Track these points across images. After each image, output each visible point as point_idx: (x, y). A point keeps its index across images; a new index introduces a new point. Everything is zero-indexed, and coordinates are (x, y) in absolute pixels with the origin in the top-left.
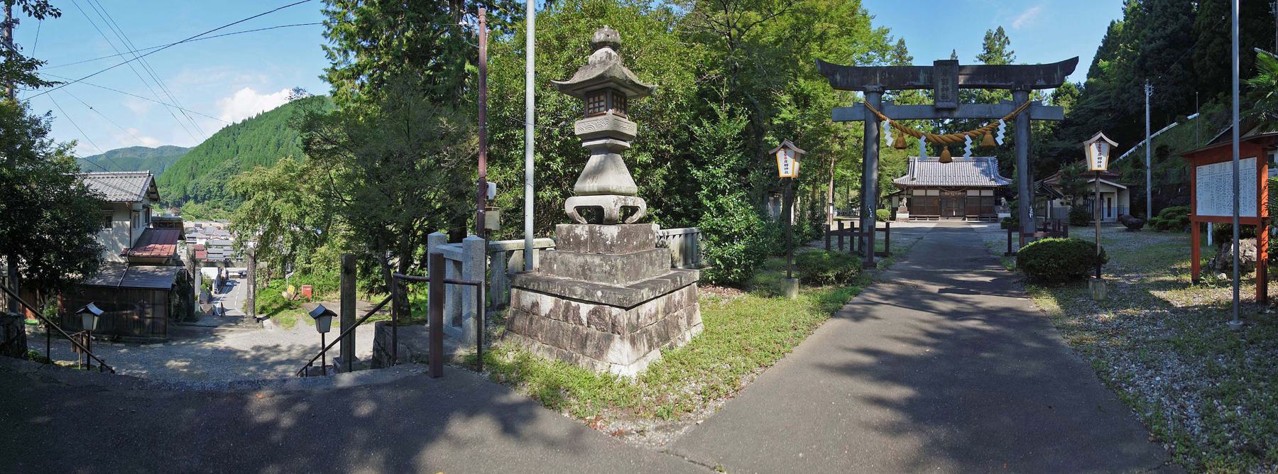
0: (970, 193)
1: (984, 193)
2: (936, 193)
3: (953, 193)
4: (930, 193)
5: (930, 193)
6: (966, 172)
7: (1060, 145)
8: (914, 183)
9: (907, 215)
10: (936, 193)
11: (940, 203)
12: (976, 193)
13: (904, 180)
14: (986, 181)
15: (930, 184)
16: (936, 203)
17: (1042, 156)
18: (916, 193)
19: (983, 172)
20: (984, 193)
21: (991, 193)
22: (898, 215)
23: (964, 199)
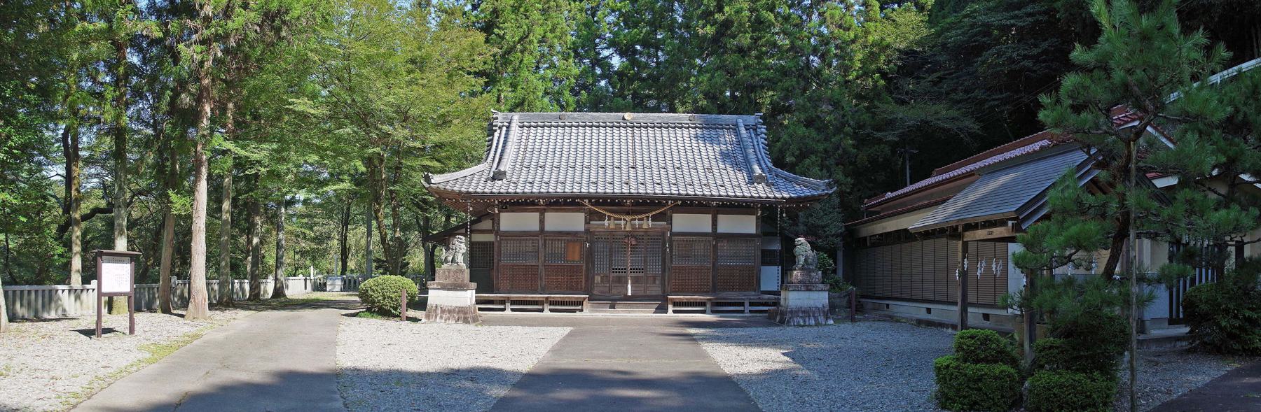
0: (682, 223)
1: (728, 224)
2: (575, 221)
3: (626, 223)
4: (557, 221)
5: (557, 221)
6: (675, 156)
7: (909, 115)
8: (499, 187)
9: (468, 297)
10: (575, 221)
11: (589, 256)
12: (702, 223)
13: (469, 179)
14: (733, 184)
15: (554, 188)
16: (575, 255)
17: (861, 142)
18: (510, 221)
19: (725, 156)
20: (728, 224)
21: (748, 225)
22: (436, 297)
23: (661, 242)
